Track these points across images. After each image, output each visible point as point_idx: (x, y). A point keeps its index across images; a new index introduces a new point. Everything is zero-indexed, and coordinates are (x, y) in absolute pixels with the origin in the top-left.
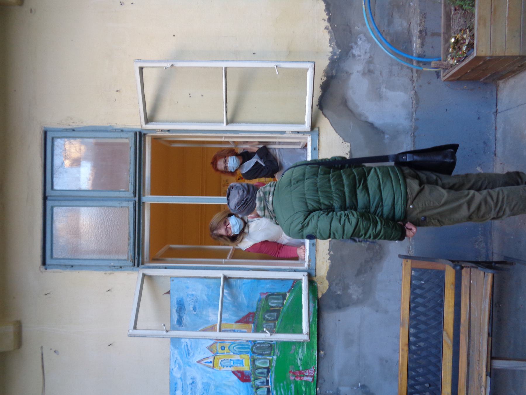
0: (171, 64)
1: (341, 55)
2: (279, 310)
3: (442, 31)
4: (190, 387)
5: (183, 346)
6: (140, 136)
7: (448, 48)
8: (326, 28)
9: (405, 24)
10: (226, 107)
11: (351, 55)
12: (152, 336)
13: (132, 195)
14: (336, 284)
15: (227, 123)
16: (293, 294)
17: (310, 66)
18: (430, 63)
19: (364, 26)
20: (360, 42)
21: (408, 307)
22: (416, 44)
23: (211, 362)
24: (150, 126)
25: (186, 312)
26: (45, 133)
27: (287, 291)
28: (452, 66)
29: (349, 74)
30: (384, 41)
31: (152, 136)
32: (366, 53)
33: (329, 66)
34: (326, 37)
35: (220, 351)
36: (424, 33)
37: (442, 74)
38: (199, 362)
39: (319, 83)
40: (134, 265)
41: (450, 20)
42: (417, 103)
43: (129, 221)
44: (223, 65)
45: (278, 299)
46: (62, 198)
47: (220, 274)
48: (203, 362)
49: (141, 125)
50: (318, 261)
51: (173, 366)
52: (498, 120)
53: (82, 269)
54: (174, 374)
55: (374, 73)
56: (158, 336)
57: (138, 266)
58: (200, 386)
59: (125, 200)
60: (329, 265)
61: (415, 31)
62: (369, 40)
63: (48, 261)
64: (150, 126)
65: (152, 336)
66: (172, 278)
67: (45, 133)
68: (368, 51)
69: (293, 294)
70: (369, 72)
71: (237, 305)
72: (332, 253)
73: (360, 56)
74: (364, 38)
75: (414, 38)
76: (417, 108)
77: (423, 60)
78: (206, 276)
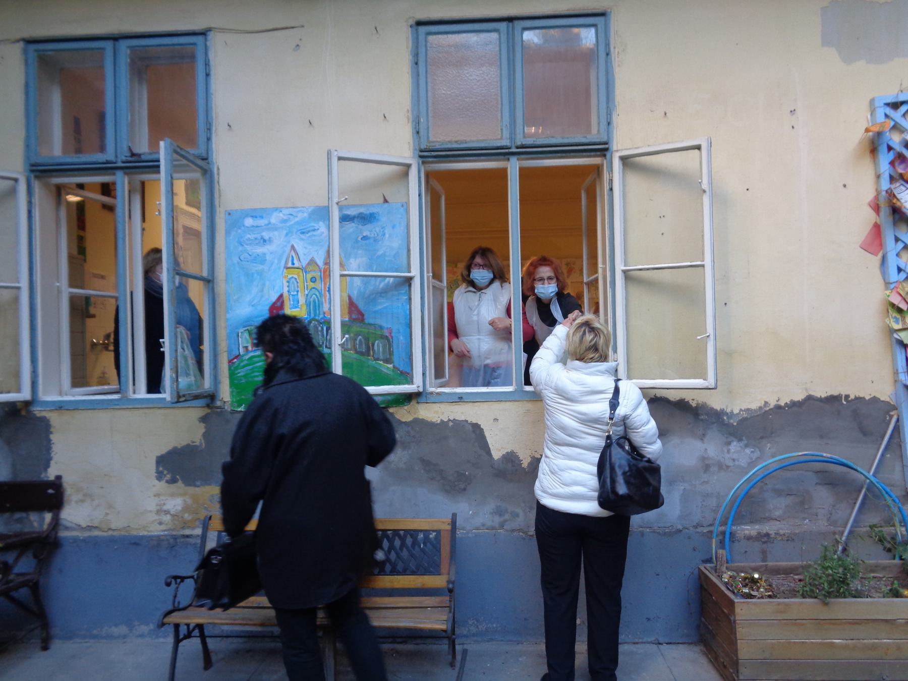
0: (707, 191)
1: (728, 425)
2: (369, 355)
3: (770, 564)
4: (259, 236)
5: (312, 224)
6: (603, 150)
7: (746, 572)
8: (766, 403)
9: (777, 513)
10: (648, 269)
11: (729, 440)
12: (330, 183)
13: (519, 143)
14: (408, 432)
15: (624, 272)
16: (391, 373)
17: (711, 382)
18: (723, 547)
19: (773, 456)
20: (748, 451)
21: (388, 528)
22: (749, 529)
23: (293, 264)
24: (617, 164)
25: (360, 227)
26: (603, 14)
27: (396, 364)
28: (720, 577)
29: (702, 438)
30: (751, 484)
31: (602, 165)
32: (734, 460)
33: (712, 409)
34: (754, 404)
35: (309, 276)
36: (765, 539)
37: (708, 565)
38: (293, 247)
39: (688, 396)
40: (421, 151)
41: (787, 574)
42: (665, 534)
43: (482, 141)
44: (708, 262)
45: (384, 352)
46: (511, 44)
47: (415, 272)
48: (293, 253)
49: (617, 151)
50: (438, 405)
51: (286, 211)
52: (647, 646)
53: (412, 77)
54: (275, 214)
55: (705, 472)
56: (330, 191)
57: (421, 157)
58: (260, 250)
59: (511, 134)
60: (434, 420)
61: (768, 528)
62: (752, 464)
63: (423, 30)
64: (617, 164)
65: (330, 183)
66: (406, 206)
67: (603, 14)
68: (737, 463)
69: (391, 373)
70: (706, 466)
71: (375, 296)
72: (451, 424)
73: (728, 452)
74: (755, 456)
75: (757, 527)
76: (659, 533)
77: (727, 539)
78: (412, 252)
